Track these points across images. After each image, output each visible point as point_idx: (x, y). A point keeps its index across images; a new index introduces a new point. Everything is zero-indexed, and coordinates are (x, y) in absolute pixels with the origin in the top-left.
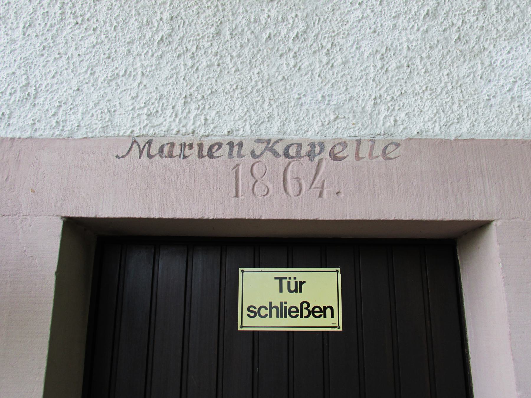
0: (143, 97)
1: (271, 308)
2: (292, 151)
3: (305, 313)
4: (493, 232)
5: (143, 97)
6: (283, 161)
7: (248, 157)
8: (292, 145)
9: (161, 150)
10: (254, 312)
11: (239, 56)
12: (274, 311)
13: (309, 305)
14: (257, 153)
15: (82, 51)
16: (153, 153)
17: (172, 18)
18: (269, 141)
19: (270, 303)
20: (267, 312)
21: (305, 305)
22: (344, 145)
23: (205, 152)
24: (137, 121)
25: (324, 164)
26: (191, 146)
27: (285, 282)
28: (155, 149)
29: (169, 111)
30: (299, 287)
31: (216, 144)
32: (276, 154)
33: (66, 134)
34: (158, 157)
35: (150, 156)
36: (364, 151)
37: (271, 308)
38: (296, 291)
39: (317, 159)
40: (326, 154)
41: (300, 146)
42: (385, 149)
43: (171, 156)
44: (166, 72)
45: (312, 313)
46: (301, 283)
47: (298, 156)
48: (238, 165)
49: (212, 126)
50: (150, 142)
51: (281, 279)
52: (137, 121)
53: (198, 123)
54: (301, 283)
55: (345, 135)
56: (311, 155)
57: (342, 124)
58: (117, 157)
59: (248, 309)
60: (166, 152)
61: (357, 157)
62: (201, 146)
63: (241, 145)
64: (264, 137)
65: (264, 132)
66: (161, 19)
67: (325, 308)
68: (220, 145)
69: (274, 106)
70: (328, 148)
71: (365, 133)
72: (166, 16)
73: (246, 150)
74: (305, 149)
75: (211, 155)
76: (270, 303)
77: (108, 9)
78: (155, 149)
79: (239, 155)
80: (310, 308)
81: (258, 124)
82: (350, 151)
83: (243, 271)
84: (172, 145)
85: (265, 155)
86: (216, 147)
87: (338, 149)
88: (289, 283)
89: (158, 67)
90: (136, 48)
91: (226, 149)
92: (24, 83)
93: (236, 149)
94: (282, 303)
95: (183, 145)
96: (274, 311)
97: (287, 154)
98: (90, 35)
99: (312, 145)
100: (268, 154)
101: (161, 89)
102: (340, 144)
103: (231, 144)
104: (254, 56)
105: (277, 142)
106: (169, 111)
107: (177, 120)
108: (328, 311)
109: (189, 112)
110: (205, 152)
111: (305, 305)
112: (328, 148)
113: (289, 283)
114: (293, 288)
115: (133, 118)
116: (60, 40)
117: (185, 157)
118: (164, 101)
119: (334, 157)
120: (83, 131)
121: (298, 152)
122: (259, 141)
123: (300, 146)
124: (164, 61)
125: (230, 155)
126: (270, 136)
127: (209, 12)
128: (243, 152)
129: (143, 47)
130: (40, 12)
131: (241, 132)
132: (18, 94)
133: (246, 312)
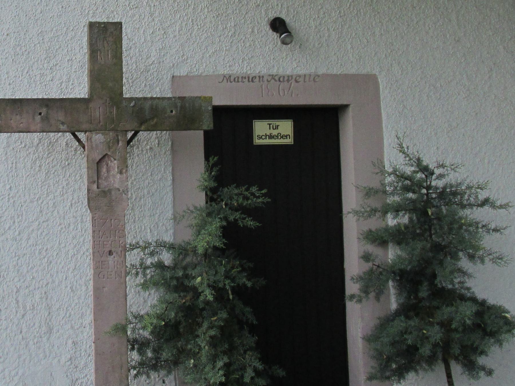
0: (227, 60)
1: (266, 136)
2: (281, 79)
3: (279, 137)
4: (350, 109)
5: (227, 60)
6: (278, 83)
7: (266, 82)
8: (281, 77)
9: (235, 79)
10: (260, 137)
11: (261, 41)
12: (267, 137)
13: (281, 134)
14: (269, 80)
15: (202, 40)
16: (232, 81)
17: (235, 25)
18: (273, 75)
19: (266, 134)
20: (265, 137)
21: (279, 134)
22: (300, 76)
23: (250, 80)
24: (225, 68)
25: (293, 83)
26: (245, 78)
27: (271, 125)
28: (232, 79)
29: (237, 64)
30: (277, 127)
31: (254, 77)
32: (276, 80)
33: (199, 74)
34: (233, 82)
35: (231, 82)
36: (307, 79)
37: (266, 136)
38: (276, 129)
39: (290, 82)
40: (293, 80)
41: (284, 77)
42: (314, 78)
43: (238, 82)
44: (234, 48)
45: (282, 137)
46: (278, 126)
47: (284, 81)
48: (262, 85)
49: (253, 70)
50: (230, 76)
51: (270, 124)
52: (225, 68)
53: (247, 69)
54: (278, 126)
55: (300, 73)
56: (288, 81)
57: (299, 68)
58: (219, 82)
59: (258, 136)
60: (236, 79)
61: (305, 82)
62: (249, 77)
63: (263, 77)
64: (271, 74)
65: (271, 72)
66: (231, 26)
67: (287, 135)
68: (255, 77)
69: (275, 62)
70: (294, 77)
71: (307, 72)
72: (233, 24)
73: (265, 79)
74: (286, 79)
75: (252, 81)
76: (266, 134)
77: (210, 22)
78: (232, 79)
79: (263, 81)
80: (281, 136)
81: (269, 69)
82: (301, 80)
83: (255, 122)
84: (238, 78)
85: (272, 81)
86: (254, 78)
87: (298, 78)
88: (273, 126)
89: (231, 46)
90: (222, 38)
91: (258, 78)
92: (182, 54)
93: (261, 78)
94: (270, 134)
95: (242, 77)
96: (267, 137)
97: (279, 81)
98: (204, 33)
99: (288, 77)
100: (273, 81)
101: (233, 55)
102: (298, 76)
103: (259, 77)
104: (266, 41)
105: (276, 76)
106: (237, 64)
107: (240, 68)
108: (288, 137)
109: (244, 65)
110: (250, 80)
111: (279, 134)
112: (294, 77)
113: (273, 126)
114: (274, 128)
115: (224, 68)
116: (193, 35)
117: (243, 82)
118: (235, 60)
119: (296, 81)
120: (206, 72)
121: (283, 79)
122: (270, 75)
123: (284, 77)
124: (233, 44)
125: (259, 81)
126: (273, 74)
127: (248, 22)
128: (264, 80)
129: (225, 38)
130: (184, 24)
131: (263, 72)
132: (181, 59)
133: (256, 137)
